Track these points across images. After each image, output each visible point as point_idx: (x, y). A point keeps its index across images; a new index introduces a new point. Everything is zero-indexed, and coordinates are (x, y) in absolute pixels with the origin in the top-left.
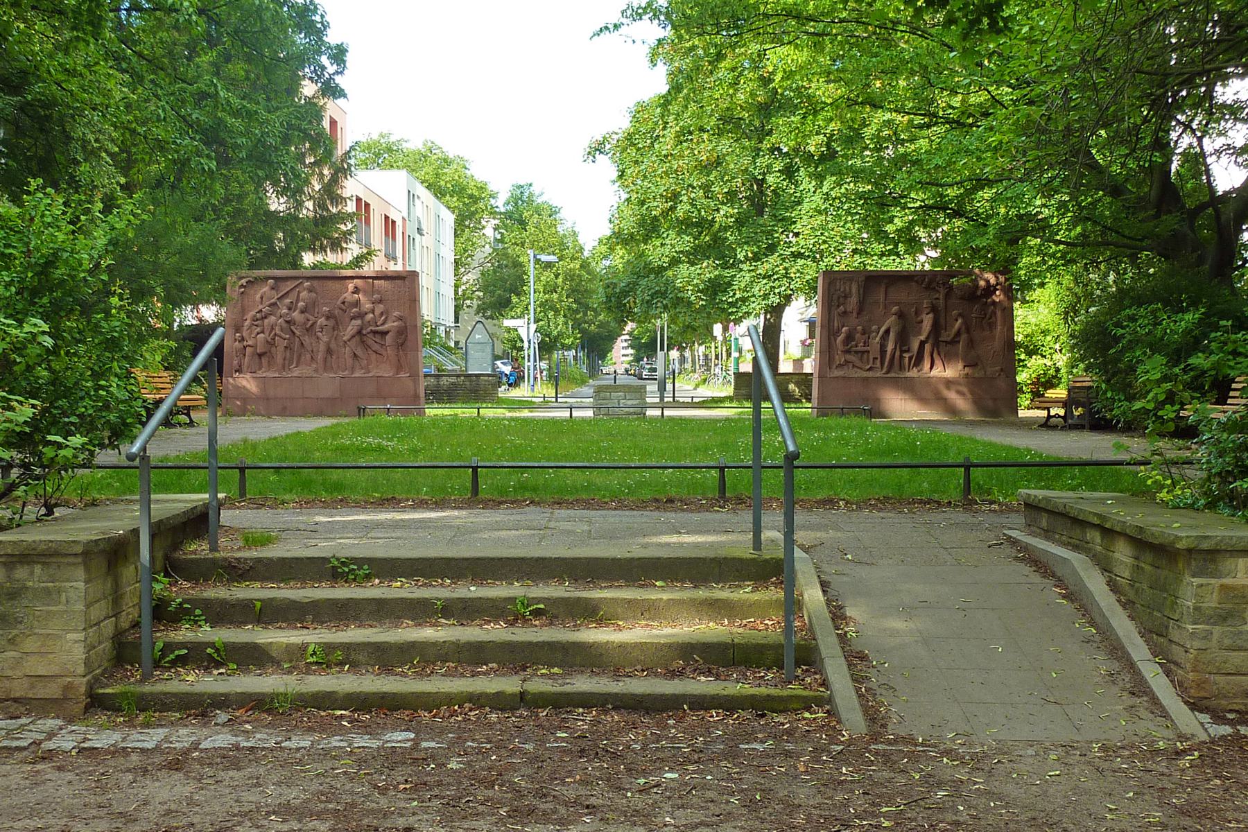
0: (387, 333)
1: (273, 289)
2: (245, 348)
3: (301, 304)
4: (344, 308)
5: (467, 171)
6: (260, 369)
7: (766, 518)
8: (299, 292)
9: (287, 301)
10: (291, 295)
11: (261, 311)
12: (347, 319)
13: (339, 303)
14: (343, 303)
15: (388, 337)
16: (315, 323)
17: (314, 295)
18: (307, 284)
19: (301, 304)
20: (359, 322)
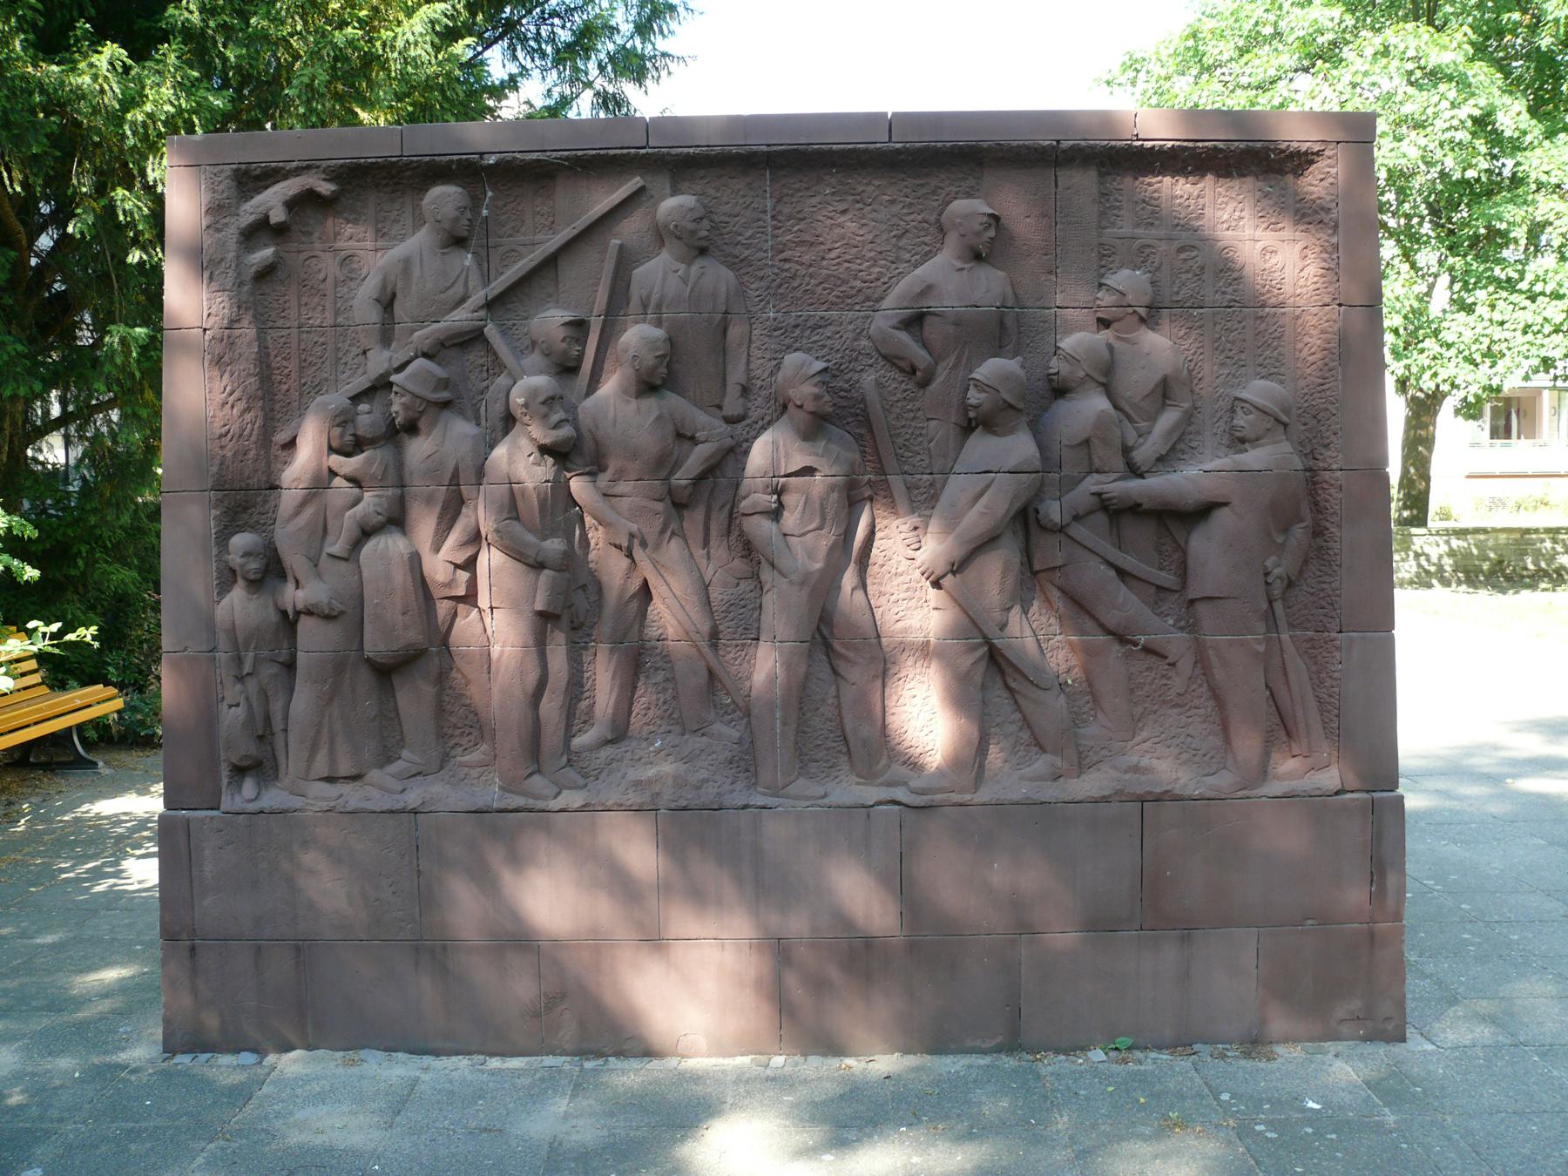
0: (1203, 511)
1: (458, 241)
2: (288, 622)
3: (636, 336)
4: (920, 356)
5: (547, 438)
6: (386, 757)
7: (714, 516)
8: (625, 262)
9: (550, 320)
10: (572, 273)
11: (381, 386)
12: (940, 430)
13: (883, 321)
14: (915, 322)
15: (1205, 545)
16: (736, 452)
17: (716, 276)
18: (673, 205)
19: (636, 336)
20: (1019, 447)
